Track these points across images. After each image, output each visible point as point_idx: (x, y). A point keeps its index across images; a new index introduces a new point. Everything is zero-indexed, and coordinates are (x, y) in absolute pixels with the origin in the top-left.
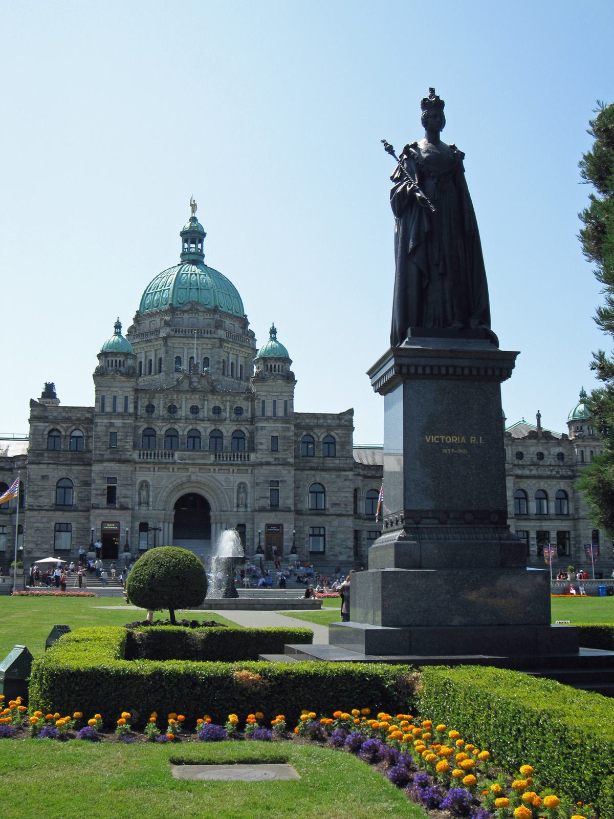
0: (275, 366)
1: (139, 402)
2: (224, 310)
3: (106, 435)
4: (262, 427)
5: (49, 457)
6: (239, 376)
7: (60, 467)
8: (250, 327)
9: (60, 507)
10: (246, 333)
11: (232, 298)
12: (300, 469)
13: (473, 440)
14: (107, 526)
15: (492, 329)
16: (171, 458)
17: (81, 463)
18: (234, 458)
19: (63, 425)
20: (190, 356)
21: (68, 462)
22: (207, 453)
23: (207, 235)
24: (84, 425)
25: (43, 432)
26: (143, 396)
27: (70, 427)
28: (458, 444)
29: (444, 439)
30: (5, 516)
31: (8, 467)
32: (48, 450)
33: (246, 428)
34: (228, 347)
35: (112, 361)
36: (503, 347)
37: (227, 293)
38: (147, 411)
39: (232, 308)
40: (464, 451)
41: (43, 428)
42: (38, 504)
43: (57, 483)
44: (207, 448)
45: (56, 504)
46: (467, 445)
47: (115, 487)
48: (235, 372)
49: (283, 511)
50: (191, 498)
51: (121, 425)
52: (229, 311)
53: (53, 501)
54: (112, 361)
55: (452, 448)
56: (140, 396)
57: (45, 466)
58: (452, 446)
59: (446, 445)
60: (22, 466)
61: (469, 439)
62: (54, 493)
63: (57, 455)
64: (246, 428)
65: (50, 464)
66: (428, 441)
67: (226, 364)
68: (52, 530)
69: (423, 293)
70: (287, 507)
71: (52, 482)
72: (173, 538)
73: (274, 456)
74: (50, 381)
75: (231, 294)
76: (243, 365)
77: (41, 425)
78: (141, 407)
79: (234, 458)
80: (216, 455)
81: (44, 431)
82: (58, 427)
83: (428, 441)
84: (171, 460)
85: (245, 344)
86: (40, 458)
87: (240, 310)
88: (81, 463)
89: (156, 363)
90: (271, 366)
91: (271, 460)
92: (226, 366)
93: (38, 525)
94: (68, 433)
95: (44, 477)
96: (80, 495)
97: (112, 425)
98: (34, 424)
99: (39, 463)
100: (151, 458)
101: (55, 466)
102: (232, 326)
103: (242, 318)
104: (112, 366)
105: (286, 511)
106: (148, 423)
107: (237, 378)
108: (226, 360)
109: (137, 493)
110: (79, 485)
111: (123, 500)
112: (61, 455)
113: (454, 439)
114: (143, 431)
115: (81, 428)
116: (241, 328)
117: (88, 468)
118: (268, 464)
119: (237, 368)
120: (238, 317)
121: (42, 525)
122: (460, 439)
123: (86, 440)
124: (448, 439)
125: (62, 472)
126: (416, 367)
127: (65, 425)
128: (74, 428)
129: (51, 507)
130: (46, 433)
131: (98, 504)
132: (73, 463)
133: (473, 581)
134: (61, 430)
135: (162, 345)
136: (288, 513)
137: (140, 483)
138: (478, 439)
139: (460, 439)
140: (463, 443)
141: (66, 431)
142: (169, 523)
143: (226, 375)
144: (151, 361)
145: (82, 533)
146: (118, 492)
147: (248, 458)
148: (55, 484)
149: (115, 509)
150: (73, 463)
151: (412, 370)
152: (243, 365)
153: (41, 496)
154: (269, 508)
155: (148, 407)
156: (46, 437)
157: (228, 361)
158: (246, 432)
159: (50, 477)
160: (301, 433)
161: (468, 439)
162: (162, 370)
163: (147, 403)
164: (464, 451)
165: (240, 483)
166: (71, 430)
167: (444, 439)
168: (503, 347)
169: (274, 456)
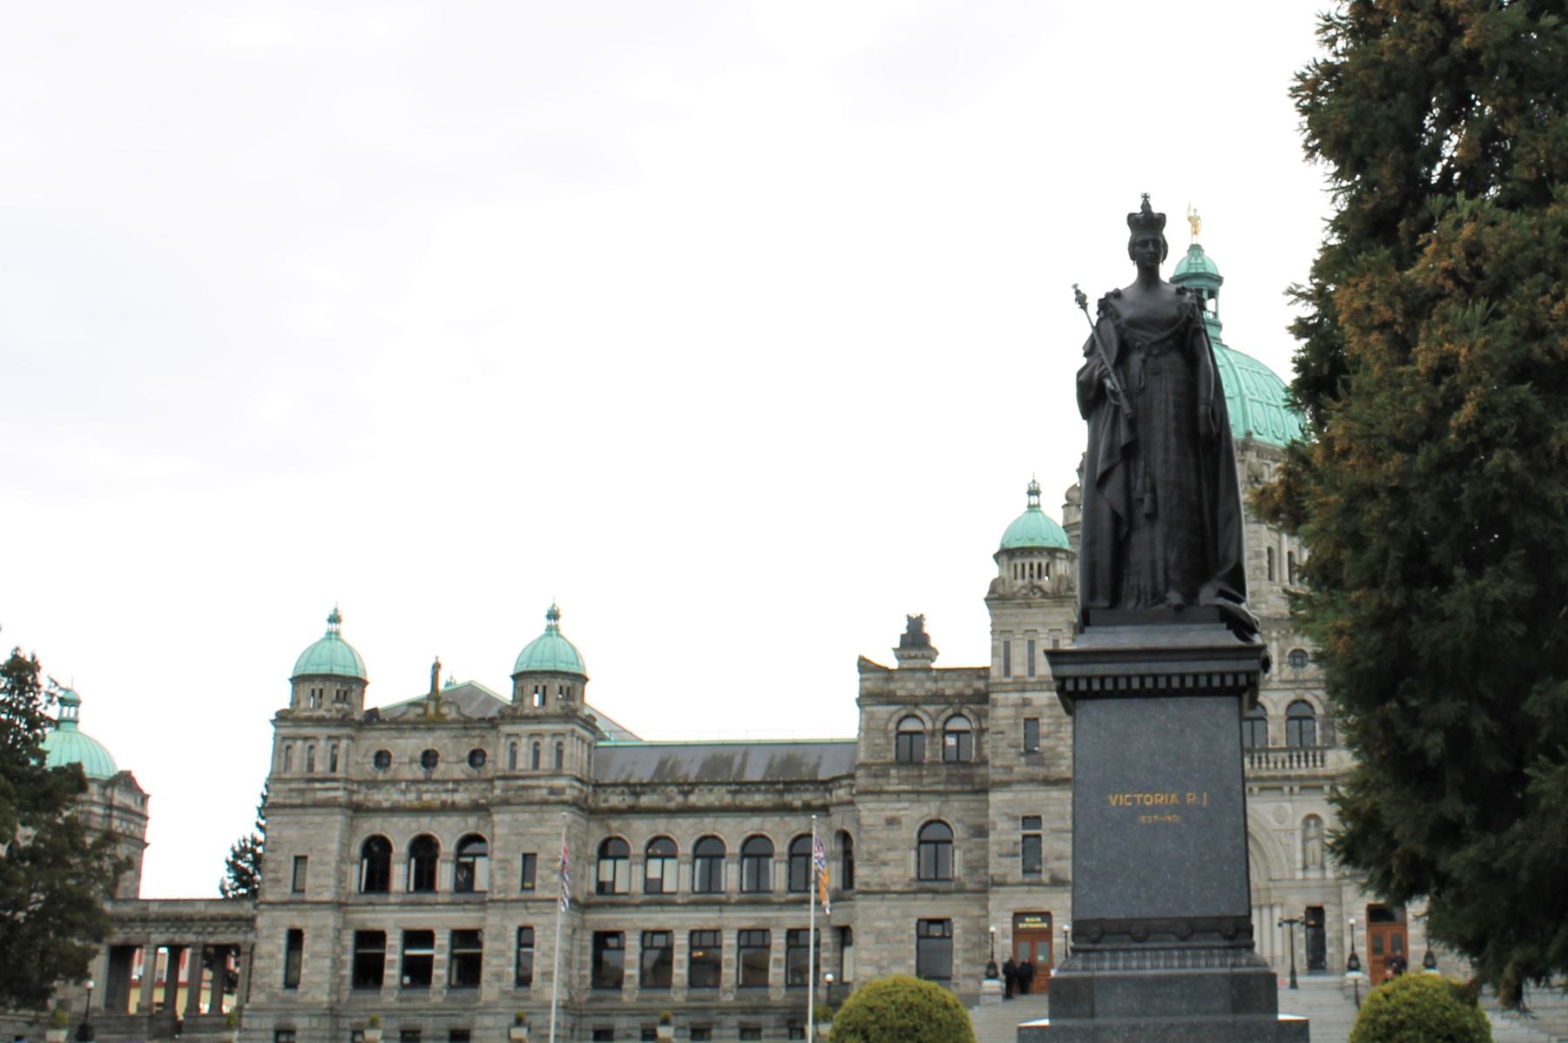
5: (899, 777)
7: (923, 797)
9: (928, 885)
13: (1191, 798)
17: (968, 788)
19: (927, 708)
21: (941, 787)
24: (971, 706)
25: (887, 724)
27: (943, 711)
29: (1142, 799)
32: (899, 763)
33: (1317, 697)
41: (886, 716)
42: (881, 880)
43: (920, 833)
45: (919, 879)
46: (1180, 808)
53: (913, 873)
58: (1155, 809)
59: (1144, 810)
60: (847, 798)
62: (913, 854)
64: (1317, 697)
66: (1114, 804)
68: (910, 936)
69: (1120, 549)
71: (909, 832)
74: (914, 614)
77: (883, 711)
81: (889, 720)
82: (918, 712)
86: (880, 781)
93: (881, 924)
94: (939, 725)
95: (892, 822)
96: (969, 856)
98: (868, 709)
99: (880, 793)
110: (966, 836)
112: (925, 773)
115: (965, 711)
117: (981, 797)
121: (889, 924)
122: (1169, 799)
124: (1148, 800)
125: (929, 809)
127: (931, 709)
128: (950, 712)
129: (909, 885)
130: (892, 726)
134: (925, 718)
139: (1169, 799)
141: (934, 720)
145: (975, 939)
147: (1322, 761)
148: (915, 835)
151: (1083, 686)
153: (885, 863)
156: (893, 735)
158: (1315, 703)
159: (904, 820)
166: (943, 717)
167: (1142, 799)
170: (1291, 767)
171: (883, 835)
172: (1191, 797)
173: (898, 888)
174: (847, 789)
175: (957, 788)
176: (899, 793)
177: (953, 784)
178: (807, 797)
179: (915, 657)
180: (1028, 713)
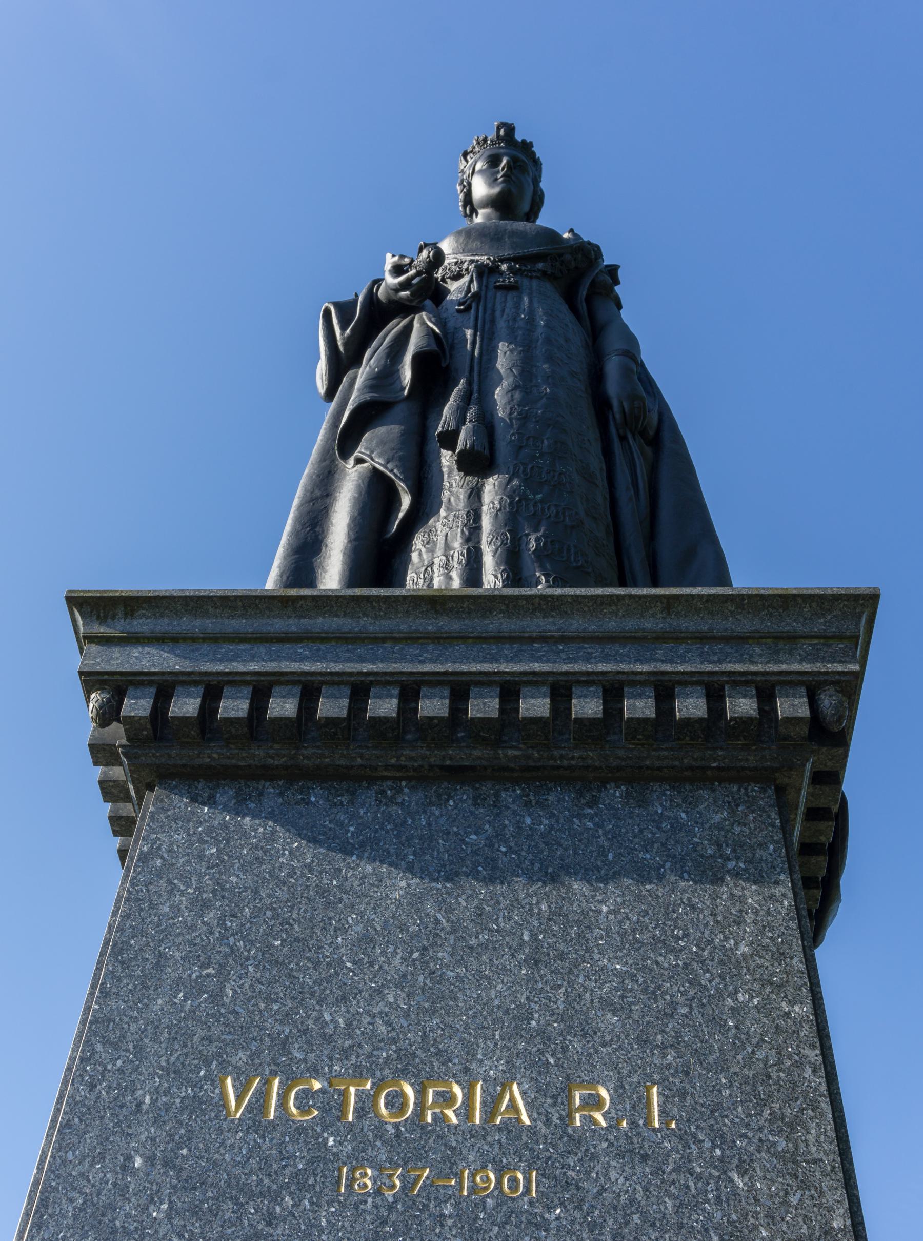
29: (366, 1106)
167: (366, 1106)
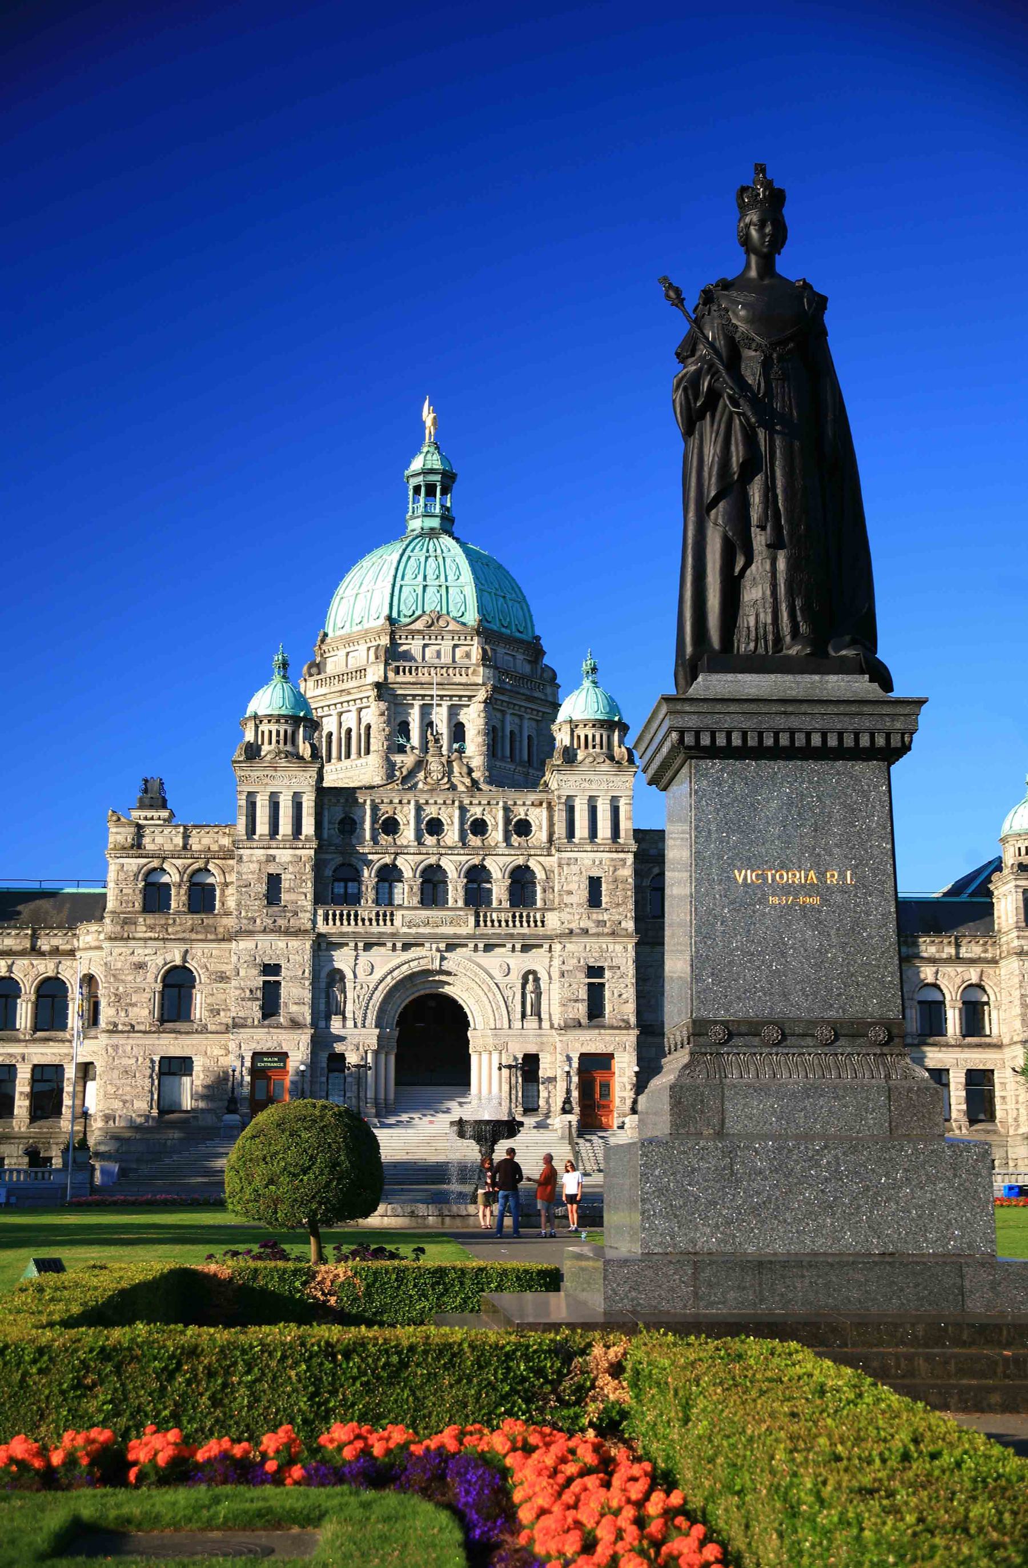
0: (594, 736)
1: (326, 813)
2: (495, 628)
3: (259, 879)
4: (570, 859)
6: (526, 757)
7: (169, 945)
8: (546, 660)
10: (539, 671)
11: (510, 603)
12: (648, 944)
13: (832, 878)
14: (264, 1062)
15: (880, 655)
16: (388, 923)
17: (212, 937)
18: (514, 922)
19: (174, 861)
20: (398, 721)
22: (461, 913)
23: (458, 479)
26: (334, 800)
28: (802, 886)
29: (773, 877)
30: (61, 1045)
31: (68, 947)
34: (503, 701)
35: (270, 732)
36: (899, 692)
37: (500, 593)
38: (342, 831)
39: (510, 623)
40: (816, 900)
44: (460, 903)
46: (821, 889)
47: (278, 983)
48: (517, 752)
49: (612, 1027)
50: (432, 1004)
51: (289, 859)
52: (504, 630)
54: (270, 732)
55: (788, 894)
56: (326, 801)
57: (141, 943)
58: (787, 889)
60: (94, 944)
61: (824, 874)
63: (163, 922)
65: (151, 939)
66: (740, 881)
67: (500, 734)
70: (623, 1020)
72: (397, 1084)
73: (594, 917)
75: (508, 596)
76: (534, 734)
78: (330, 823)
79: (514, 922)
80: (477, 916)
83: (740, 881)
84: (388, 929)
85: (537, 694)
87: (526, 627)
88: (212, 937)
89: (340, 739)
90: (586, 737)
91: (589, 924)
92: (500, 740)
95: (140, 966)
97: (272, 859)
100: (349, 924)
101: (160, 944)
102: (511, 659)
103: (528, 643)
104: (270, 743)
105: (619, 1028)
106: (342, 853)
107: (521, 763)
108: (498, 726)
109: (323, 995)
111: (293, 1008)
113: (794, 875)
114: (334, 871)
116: (529, 662)
118: (585, 932)
119: (521, 742)
120: (522, 642)
123: (223, 891)
124: (781, 876)
126: (792, 733)
127: (179, 862)
131: (245, 1019)
132: (194, 936)
133: (828, 1163)
135: (372, 699)
136: (624, 1032)
137: (328, 975)
138: (842, 875)
140: (812, 884)
142: (387, 1054)
143: (499, 755)
144: (349, 731)
146: (283, 992)
149: (279, 1026)
150: (194, 936)
152: (534, 734)
154: (584, 1021)
155: (342, 822)
157: (521, 732)
160: (650, 869)
161: (821, 875)
162: (372, 748)
163: (340, 816)
164: (816, 900)
165: (529, 972)
168: (899, 692)
169: (594, 917)
170: (514, 926)
171: (130, 978)
172: (833, 876)
173: (142, 1028)
174: (95, 935)
175: (200, 937)
176: (145, 939)
177: (197, 933)
178: (56, 942)
179: (152, 819)
180: (272, 869)
